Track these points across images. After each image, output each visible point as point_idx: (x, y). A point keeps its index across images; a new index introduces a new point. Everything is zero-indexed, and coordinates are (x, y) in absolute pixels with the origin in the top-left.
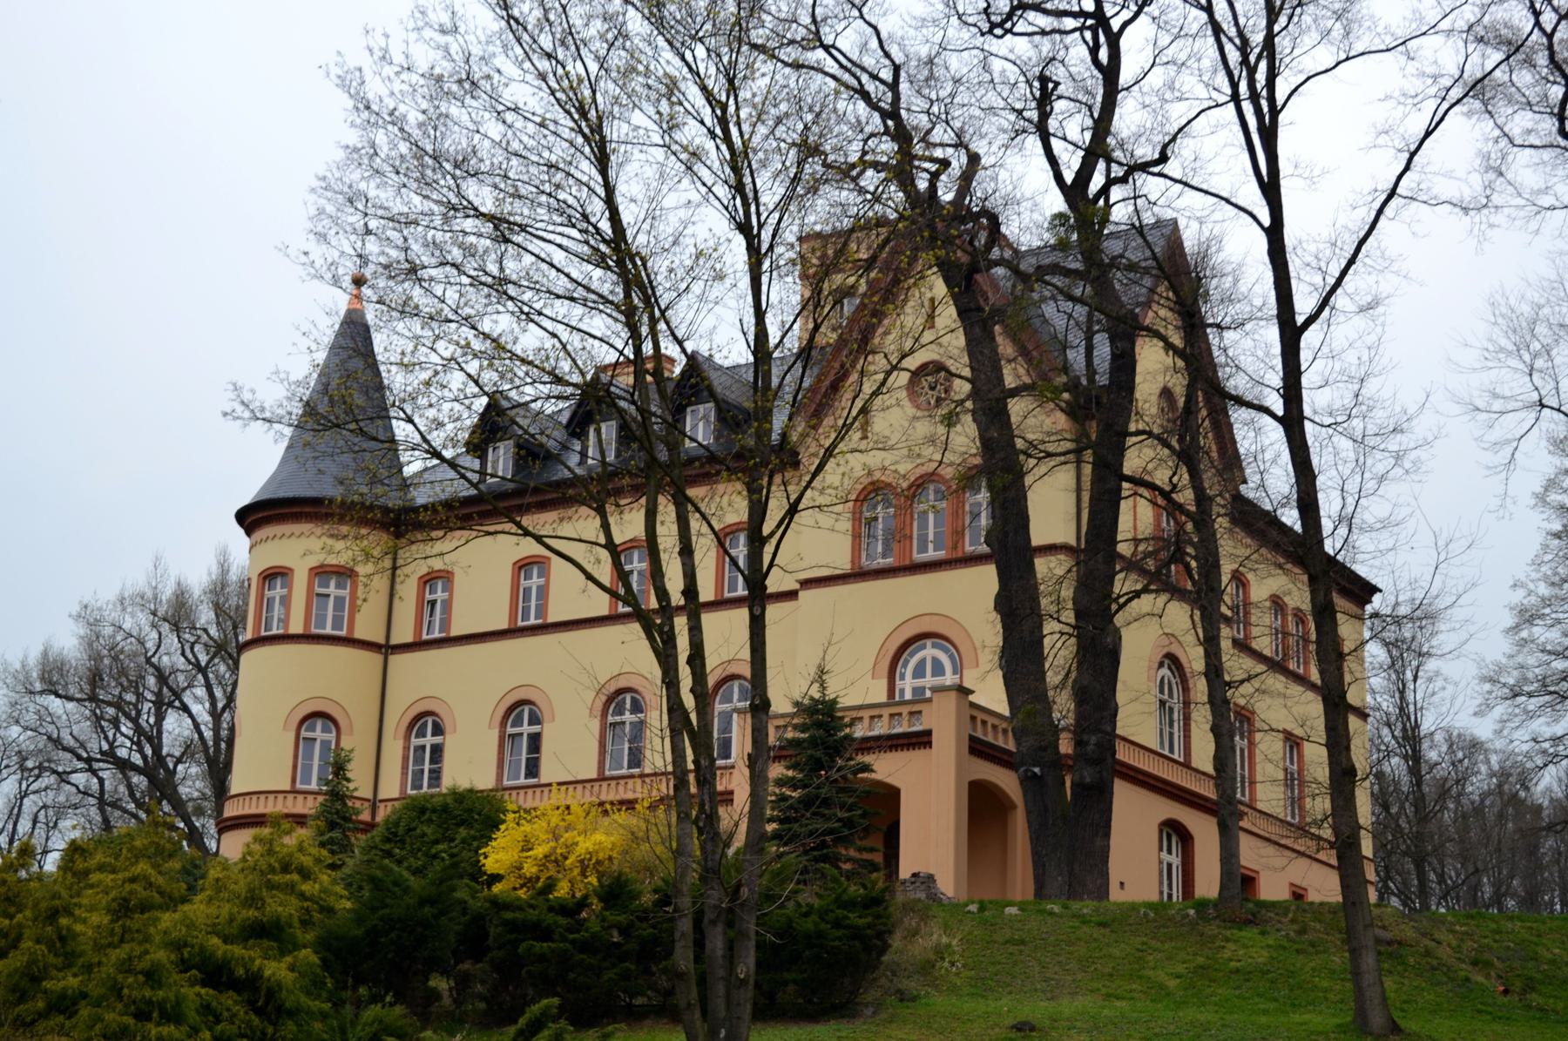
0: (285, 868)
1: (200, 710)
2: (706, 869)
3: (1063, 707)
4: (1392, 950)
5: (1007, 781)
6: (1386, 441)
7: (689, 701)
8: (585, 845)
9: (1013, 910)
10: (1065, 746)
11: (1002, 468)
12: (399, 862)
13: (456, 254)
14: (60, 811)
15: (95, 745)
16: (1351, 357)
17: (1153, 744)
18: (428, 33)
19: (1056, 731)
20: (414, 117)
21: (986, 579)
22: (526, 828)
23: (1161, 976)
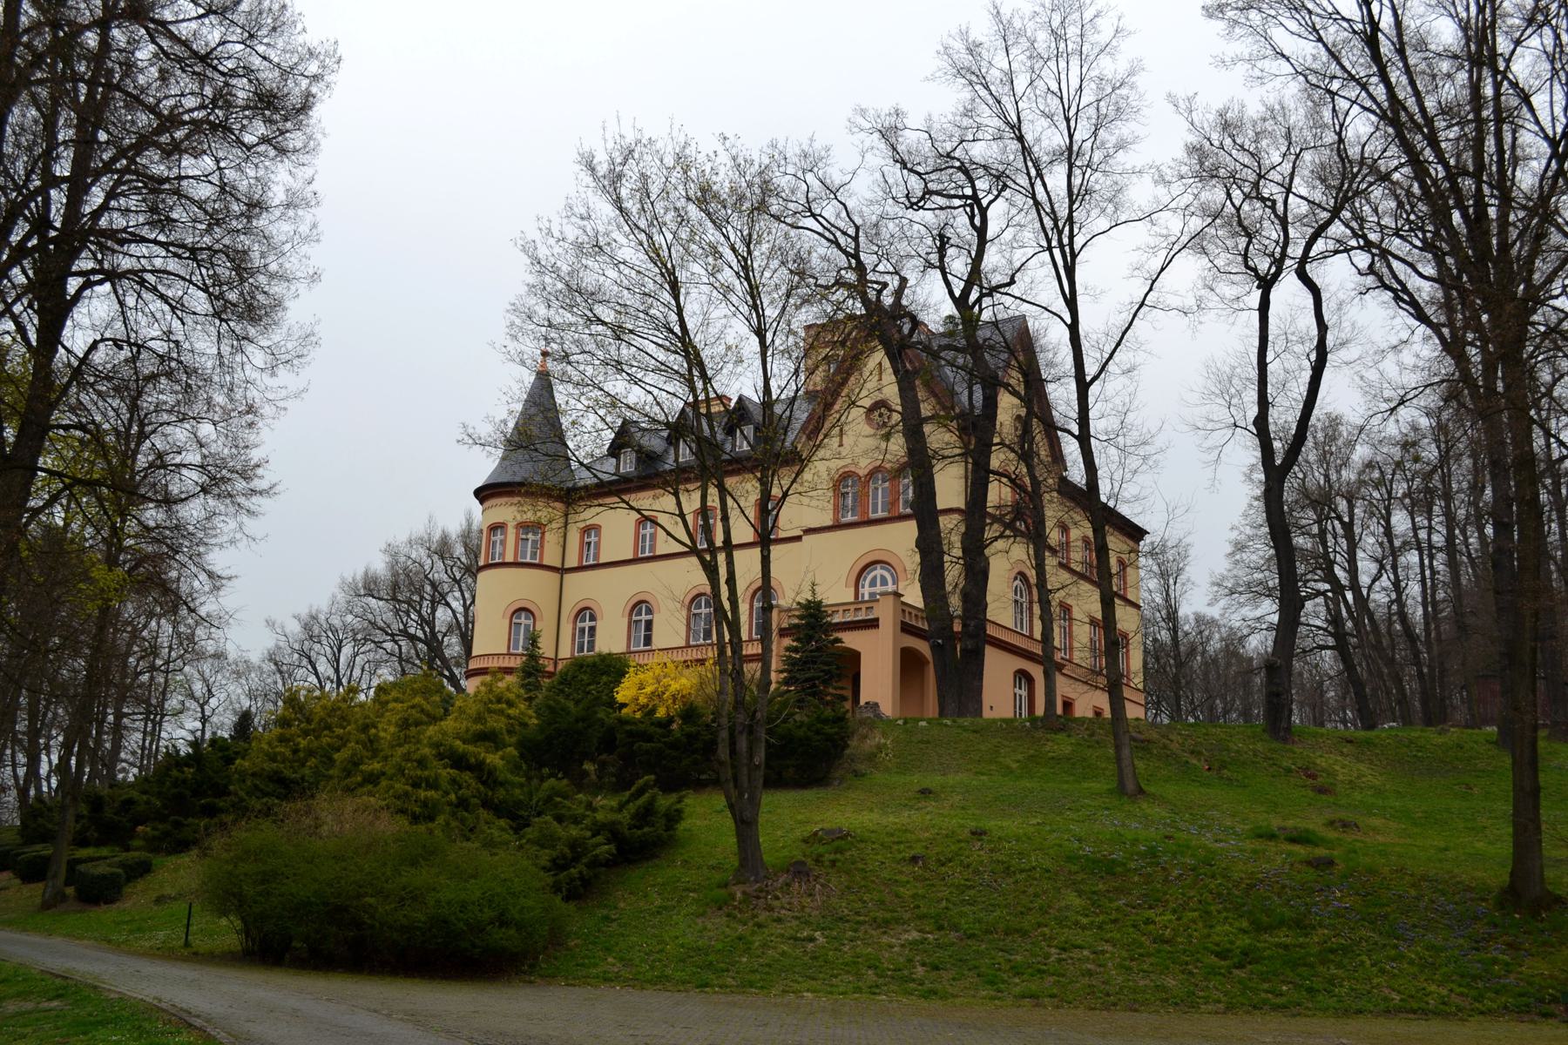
0: (499, 701)
1: (457, 605)
2: (736, 702)
3: (955, 602)
4: (1144, 746)
5: (924, 647)
6: (1138, 449)
7: (727, 605)
8: (675, 686)
9: (924, 724)
10: (957, 627)
11: (920, 464)
12: (567, 697)
13: (591, 347)
14: (378, 664)
15: (396, 626)
16: (1117, 401)
17: (1011, 625)
18: (574, 219)
19: (952, 618)
20: (565, 268)
21: (910, 530)
22: (641, 676)
23: (1008, 761)
